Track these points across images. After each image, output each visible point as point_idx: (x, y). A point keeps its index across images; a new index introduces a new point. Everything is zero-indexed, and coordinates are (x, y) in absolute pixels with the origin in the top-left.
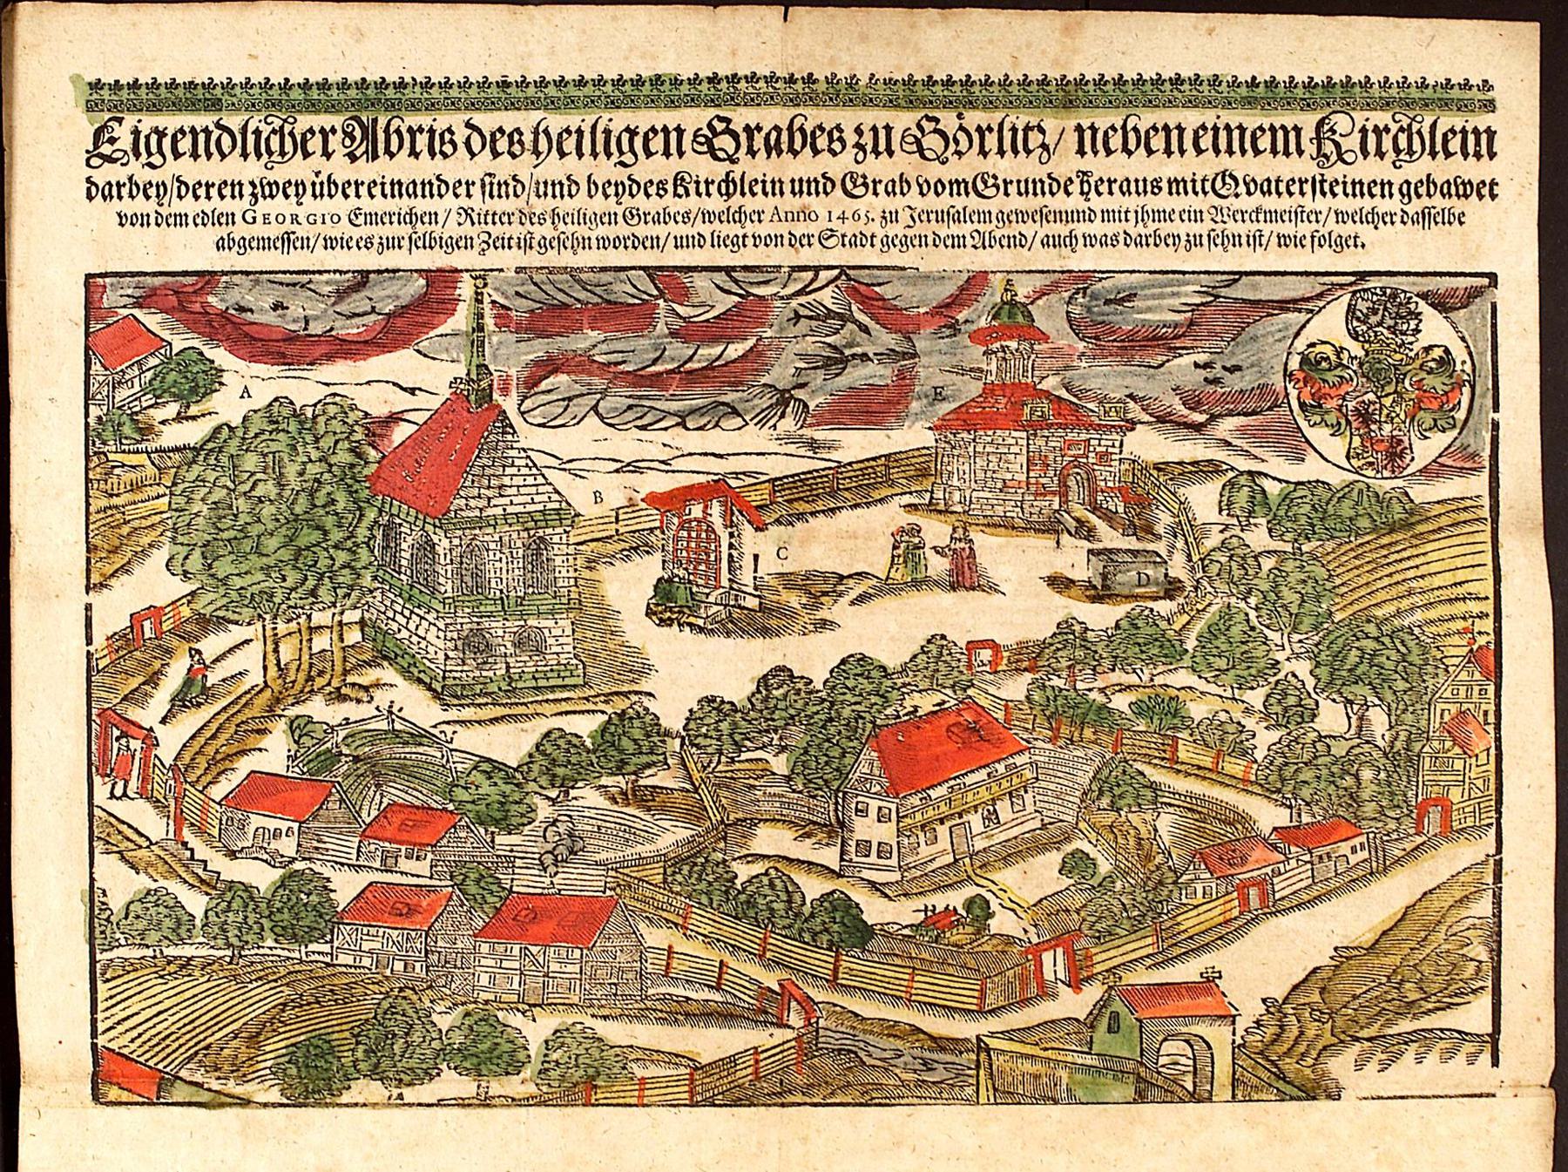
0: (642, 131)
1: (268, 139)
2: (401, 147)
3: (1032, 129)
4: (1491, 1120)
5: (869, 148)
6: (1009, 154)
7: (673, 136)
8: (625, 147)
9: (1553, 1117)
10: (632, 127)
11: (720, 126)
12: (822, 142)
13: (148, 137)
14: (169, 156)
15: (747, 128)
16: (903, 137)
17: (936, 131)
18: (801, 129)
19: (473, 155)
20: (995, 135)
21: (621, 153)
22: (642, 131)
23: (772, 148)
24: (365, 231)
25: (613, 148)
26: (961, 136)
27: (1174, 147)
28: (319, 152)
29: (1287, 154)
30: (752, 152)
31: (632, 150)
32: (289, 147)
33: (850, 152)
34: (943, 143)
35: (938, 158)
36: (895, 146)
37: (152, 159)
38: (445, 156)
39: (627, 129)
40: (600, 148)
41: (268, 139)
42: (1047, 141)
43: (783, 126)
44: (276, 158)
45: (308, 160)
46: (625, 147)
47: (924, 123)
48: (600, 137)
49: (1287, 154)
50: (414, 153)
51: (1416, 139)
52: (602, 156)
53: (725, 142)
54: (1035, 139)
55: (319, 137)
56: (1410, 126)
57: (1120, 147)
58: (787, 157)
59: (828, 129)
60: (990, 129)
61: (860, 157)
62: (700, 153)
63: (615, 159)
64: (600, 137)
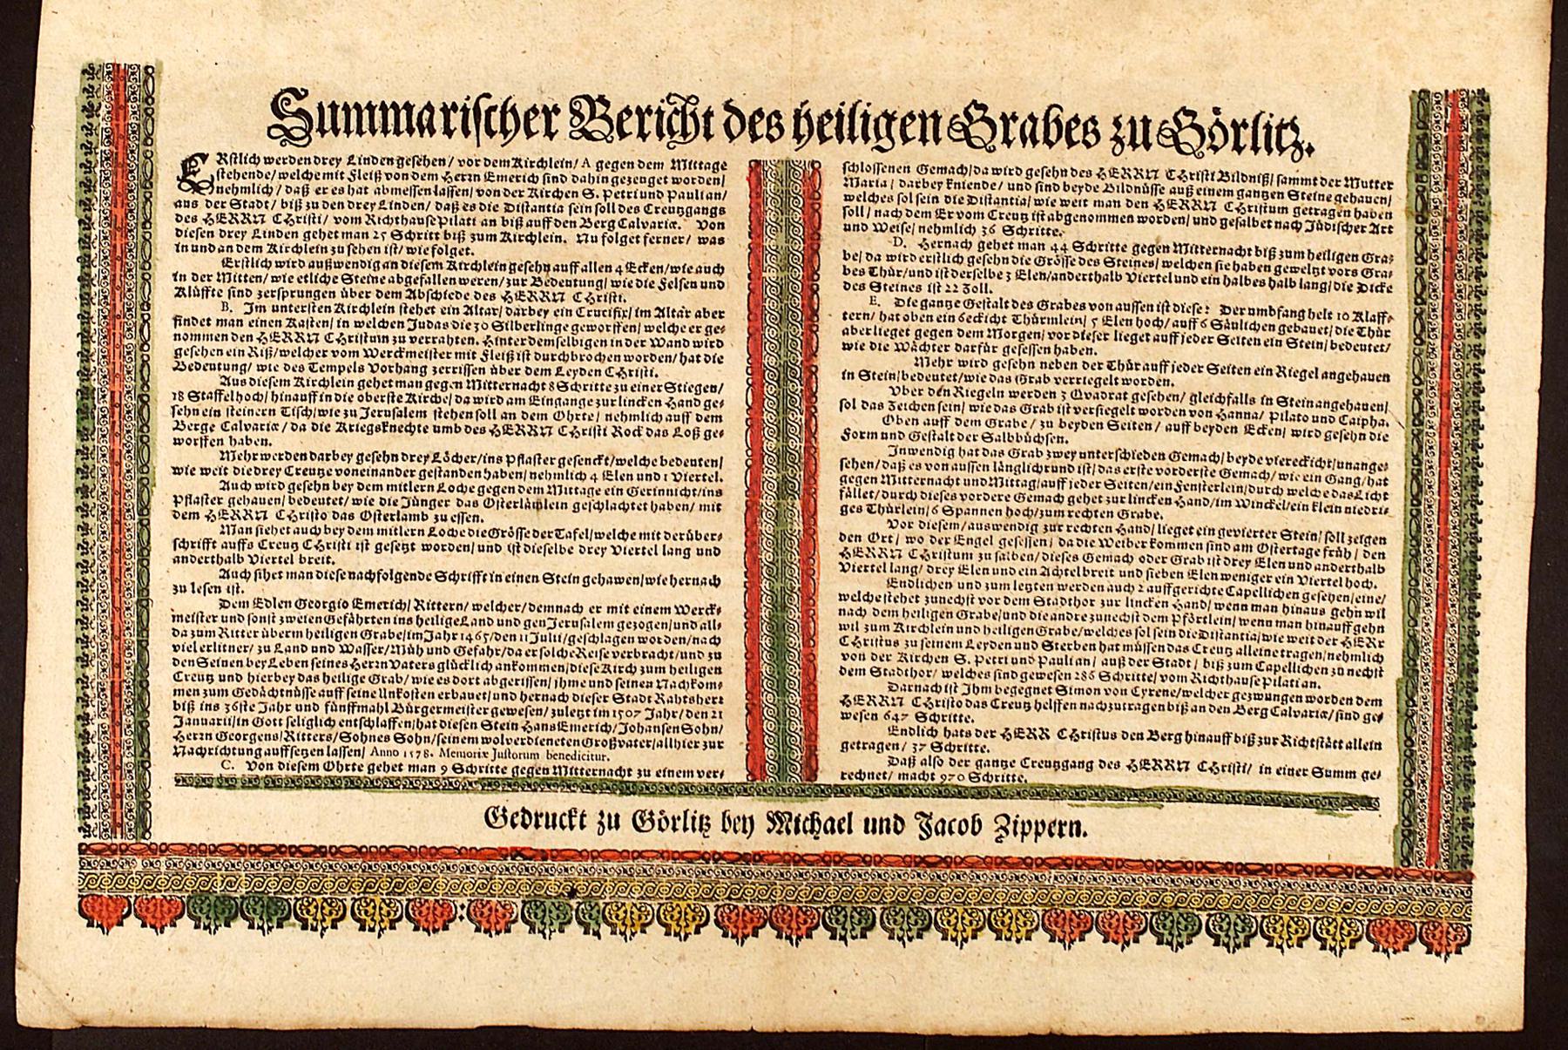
0: (899, 116)
1: (670, 119)
2: (421, 114)
3: (1285, 127)
4: (1490, 15)
5: (1127, 141)
6: (1263, 152)
7: (930, 122)
8: (883, 132)
9: (1550, 14)
10: (890, 112)
11: (976, 114)
12: (1077, 134)
13: (877, 121)
14: (898, 140)
15: (1004, 117)
16: (1160, 130)
17: (1193, 126)
18: (1057, 121)
19: (732, 137)
20: (1250, 130)
21: (879, 138)
22: (899, 116)
23: (1029, 138)
24: (1292, 543)
25: (871, 133)
26: (1217, 131)
27: (930, 135)
28: (636, 131)
29: (360, 132)
30: (1007, 141)
31: (889, 135)
32: (691, 128)
33: (1106, 144)
34: (1199, 137)
35: (606, 137)
36: (1152, 138)
37: (880, 143)
38: (1088, 145)
39: (885, 114)
40: (858, 131)
41: (670, 119)
42: (1300, 140)
43: (1040, 116)
44: (677, 138)
45: (1073, 148)
46: (883, 132)
47: (1181, 117)
48: (859, 122)
49: (360, 132)
50: (1238, 148)
51: (690, 120)
52: (860, 140)
53: (980, 130)
54: (1288, 137)
55: (635, 117)
56: (684, 108)
57: (918, 137)
58: (1041, 146)
59: (1082, 122)
60: (1245, 125)
61: (1118, 149)
62: (955, 140)
63: (873, 142)
64: (859, 122)
